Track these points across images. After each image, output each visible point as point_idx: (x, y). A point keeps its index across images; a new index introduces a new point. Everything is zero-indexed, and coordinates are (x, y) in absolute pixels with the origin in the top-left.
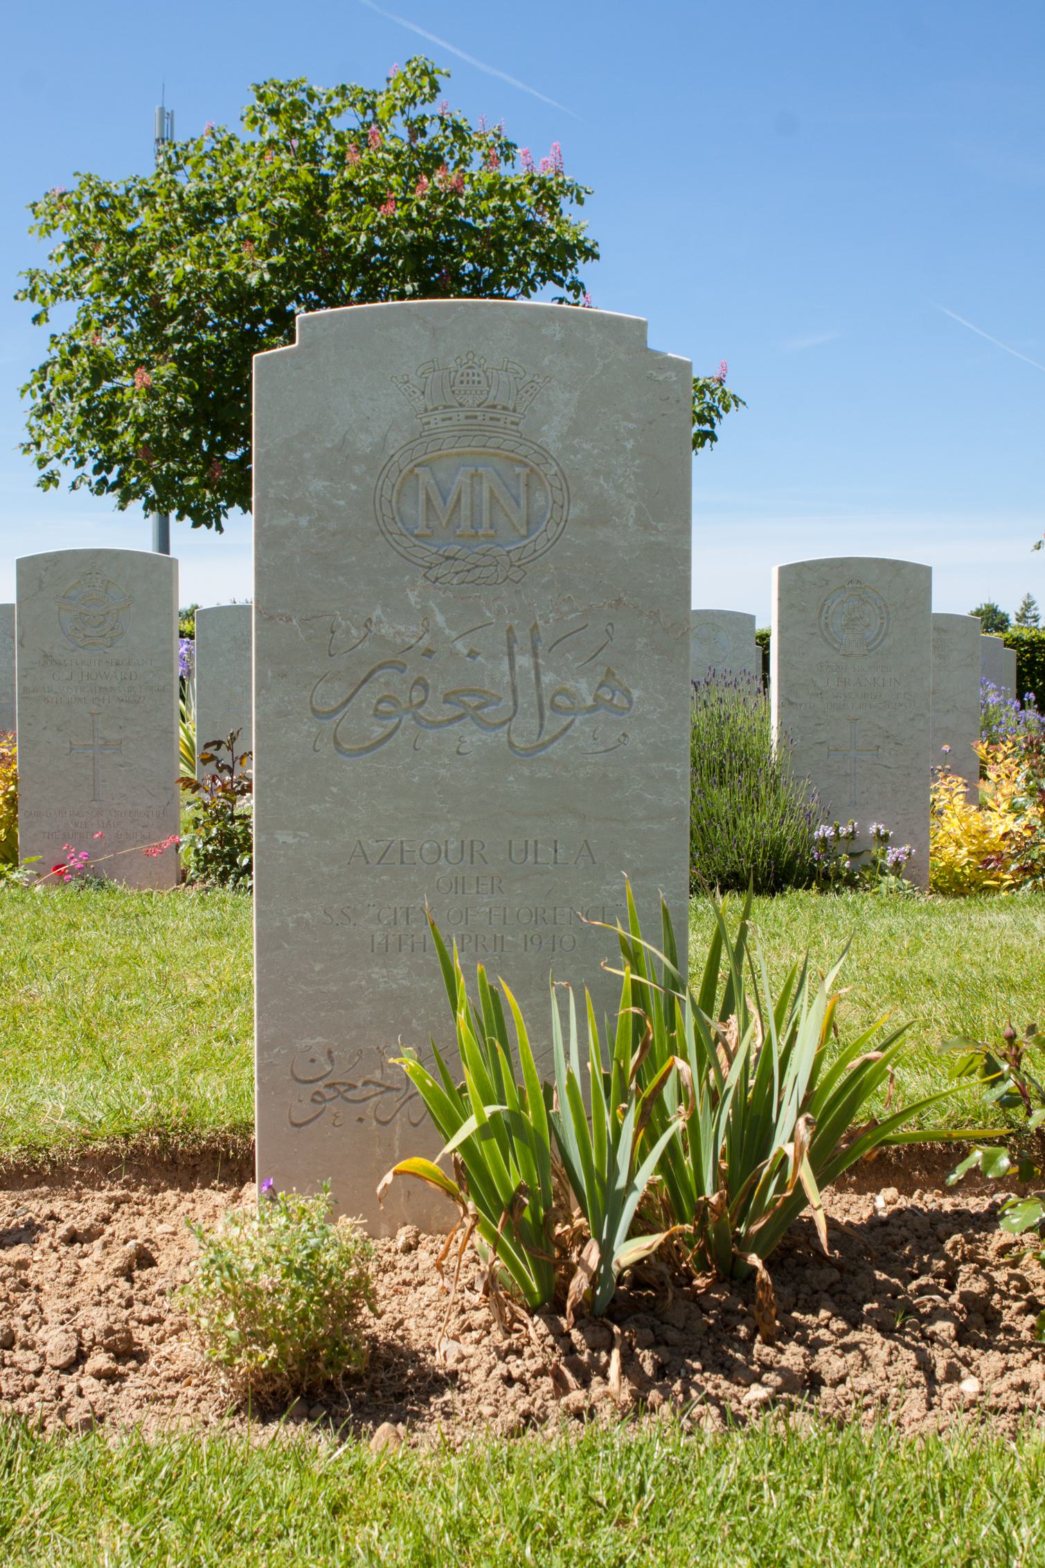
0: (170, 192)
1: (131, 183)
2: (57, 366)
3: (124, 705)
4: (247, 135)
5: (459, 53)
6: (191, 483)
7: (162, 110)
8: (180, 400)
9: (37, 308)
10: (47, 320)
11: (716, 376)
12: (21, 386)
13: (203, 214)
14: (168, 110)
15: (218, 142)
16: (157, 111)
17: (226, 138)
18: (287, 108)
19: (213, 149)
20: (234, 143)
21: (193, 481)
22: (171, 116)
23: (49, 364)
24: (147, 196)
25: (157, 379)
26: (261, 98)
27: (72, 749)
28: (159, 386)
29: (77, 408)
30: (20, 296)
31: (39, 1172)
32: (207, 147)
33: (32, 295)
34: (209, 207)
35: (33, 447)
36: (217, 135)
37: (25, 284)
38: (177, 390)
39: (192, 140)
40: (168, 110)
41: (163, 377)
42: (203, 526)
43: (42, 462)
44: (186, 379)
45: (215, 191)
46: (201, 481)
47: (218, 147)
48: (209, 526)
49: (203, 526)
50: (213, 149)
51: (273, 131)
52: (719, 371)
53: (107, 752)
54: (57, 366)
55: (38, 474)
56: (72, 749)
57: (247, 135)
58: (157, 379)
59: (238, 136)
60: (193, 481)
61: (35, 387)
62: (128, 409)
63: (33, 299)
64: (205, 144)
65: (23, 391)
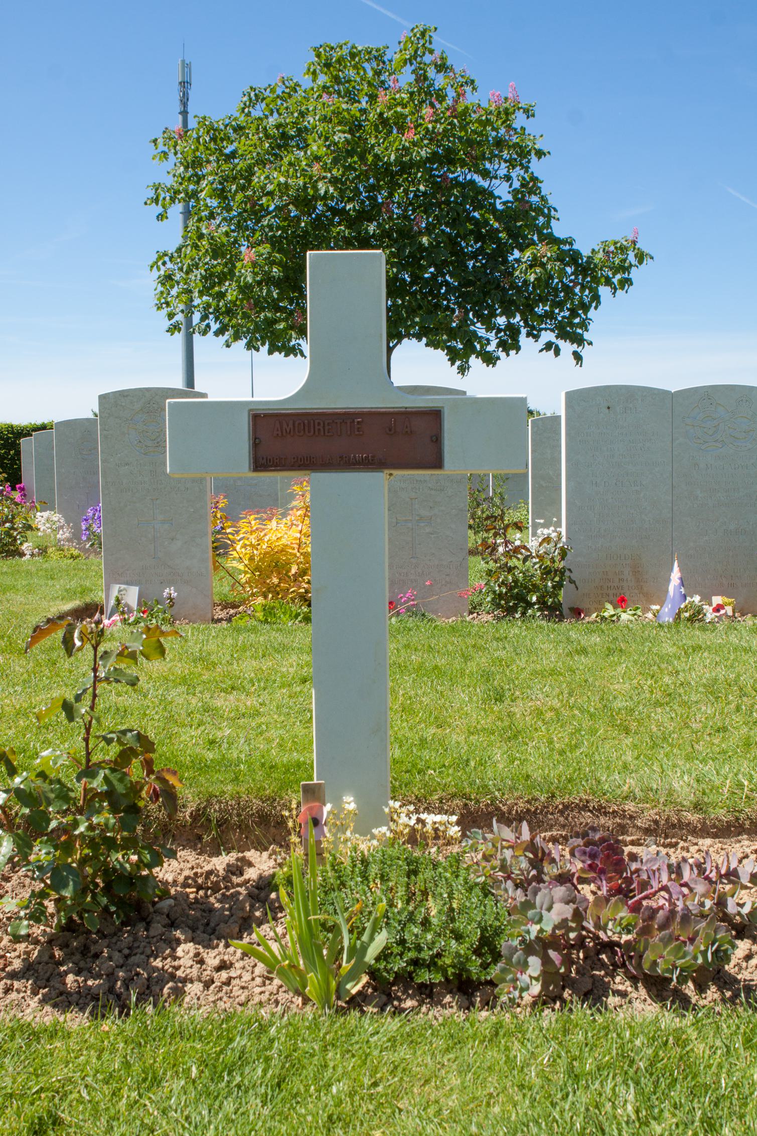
0: (258, 125)
1: (227, 121)
2: (189, 248)
3: (433, 492)
4: (306, 82)
5: (389, 14)
6: (281, 327)
7: (183, 61)
8: (275, 270)
9: (159, 209)
10: (167, 218)
11: (631, 239)
12: (151, 263)
13: (283, 141)
14: (187, 62)
15: (287, 87)
16: (180, 62)
17: (293, 85)
18: (329, 62)
19: (283, 92)
20: (298, 88)
21: (282, 326)
22: (189, 66)
23: (183, 246)
24: (239, 129)
25: (259, 256)
26: (318, 56)
27: (397, 523)
28: (261, 261)
29: (199, 276)
30: (149, 202)
31: (741, 826)
32: (279, 91)
33: (156, 201)
34: (284, 135)
35: (164, 306)
36: (286, 83)
37: (152, 194)
38: (273, 263)
39: (270, 85)
40: (187, 62)
41: (262, 255)
42: (292, 355)
43: (171, 316)
44: (277, 255)
45: (287, 124)
46: (288, 324)
47: (287, 90)
48: (296, 355)
49: (292, 355)
50: (283, 92)
51: (323, 79)
52: (632, 235)
53: (422, 524)
54: (189, 248)
55: (167, 323)
56: (397, 523)
57: (306, 82)
58: (259, 256)
59: (300, 83)
60: (282, 326)
61: (160, 263)
62: (240, 277)
63: (157, 204)
64: (278, 89)
65: (152, 267)
